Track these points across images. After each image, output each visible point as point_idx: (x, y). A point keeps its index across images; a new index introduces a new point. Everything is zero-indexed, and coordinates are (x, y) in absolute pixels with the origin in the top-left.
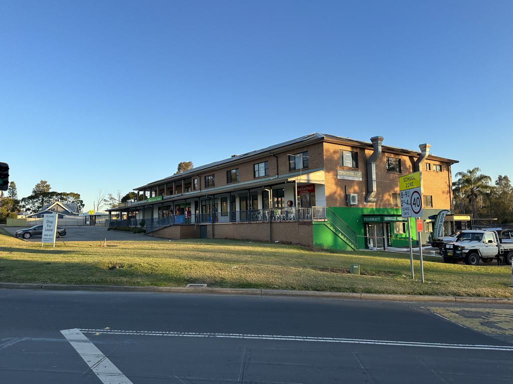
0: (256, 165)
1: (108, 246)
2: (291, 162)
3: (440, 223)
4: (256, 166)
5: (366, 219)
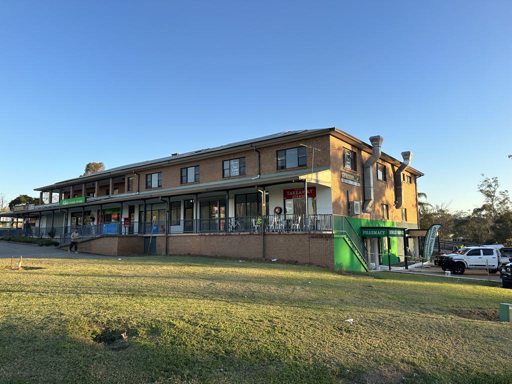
0: (183, 170)
1: (26, 268)
2: (279, 159)
3: (431, 238)
4: (226, 164)
5: (365, 232)
